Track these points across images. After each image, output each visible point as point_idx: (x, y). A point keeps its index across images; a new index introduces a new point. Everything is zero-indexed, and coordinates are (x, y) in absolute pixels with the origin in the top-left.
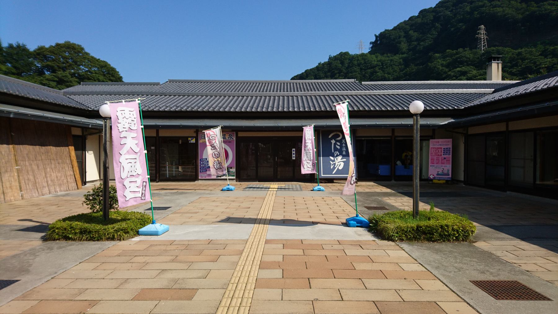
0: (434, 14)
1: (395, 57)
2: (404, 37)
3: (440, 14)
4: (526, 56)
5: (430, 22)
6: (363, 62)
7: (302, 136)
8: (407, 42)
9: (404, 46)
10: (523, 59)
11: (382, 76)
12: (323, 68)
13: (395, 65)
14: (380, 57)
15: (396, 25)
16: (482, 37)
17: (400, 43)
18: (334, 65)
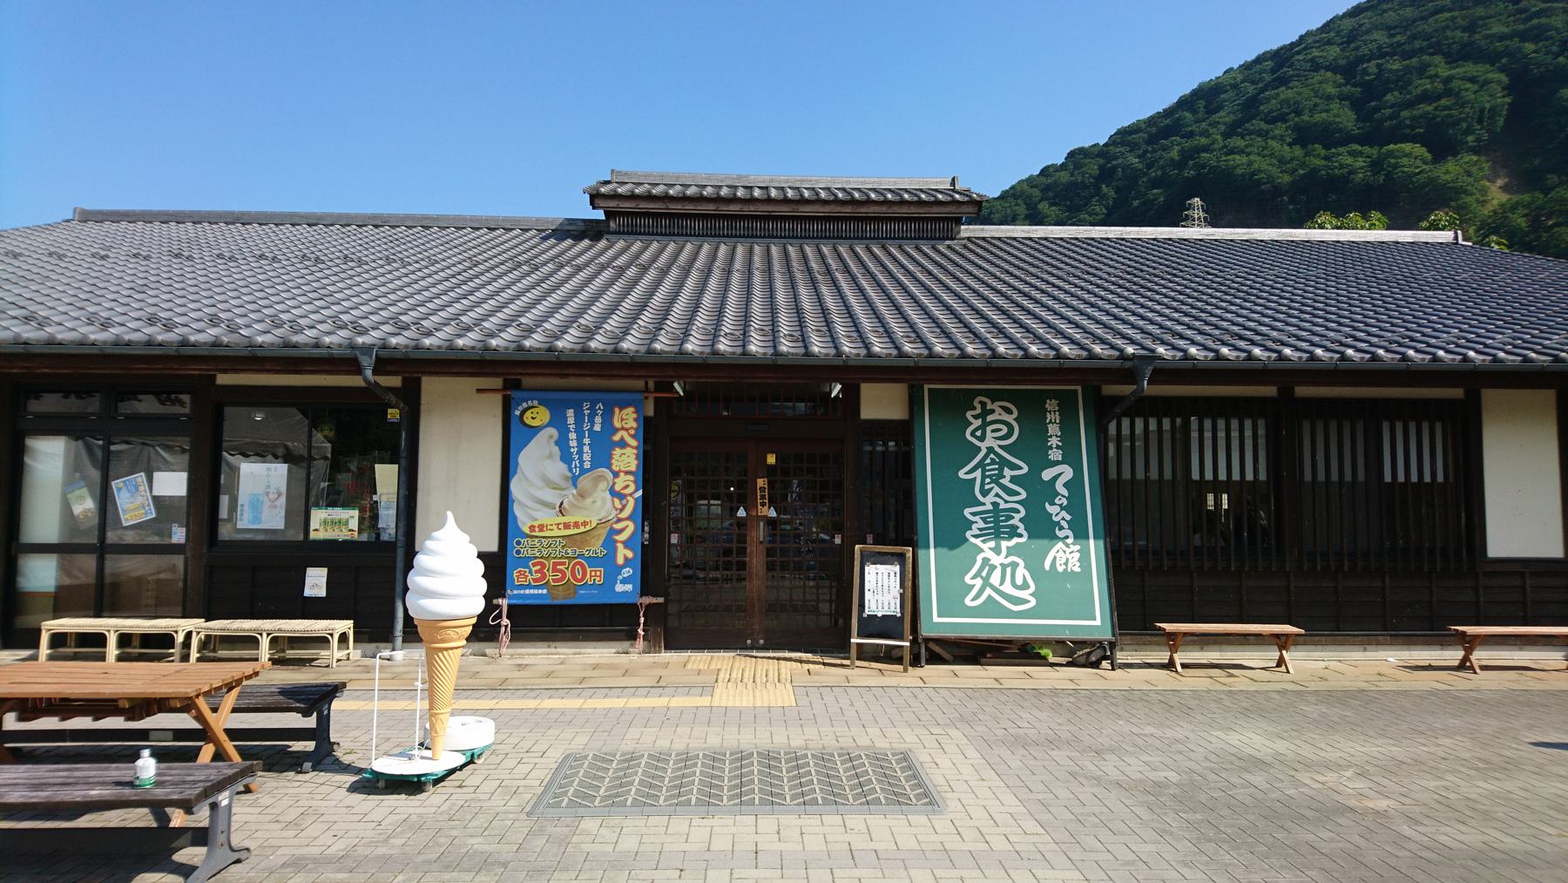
0: (1102, 161)
5: (1092, 180)
7: (289, 637)
15: (1007, 187)
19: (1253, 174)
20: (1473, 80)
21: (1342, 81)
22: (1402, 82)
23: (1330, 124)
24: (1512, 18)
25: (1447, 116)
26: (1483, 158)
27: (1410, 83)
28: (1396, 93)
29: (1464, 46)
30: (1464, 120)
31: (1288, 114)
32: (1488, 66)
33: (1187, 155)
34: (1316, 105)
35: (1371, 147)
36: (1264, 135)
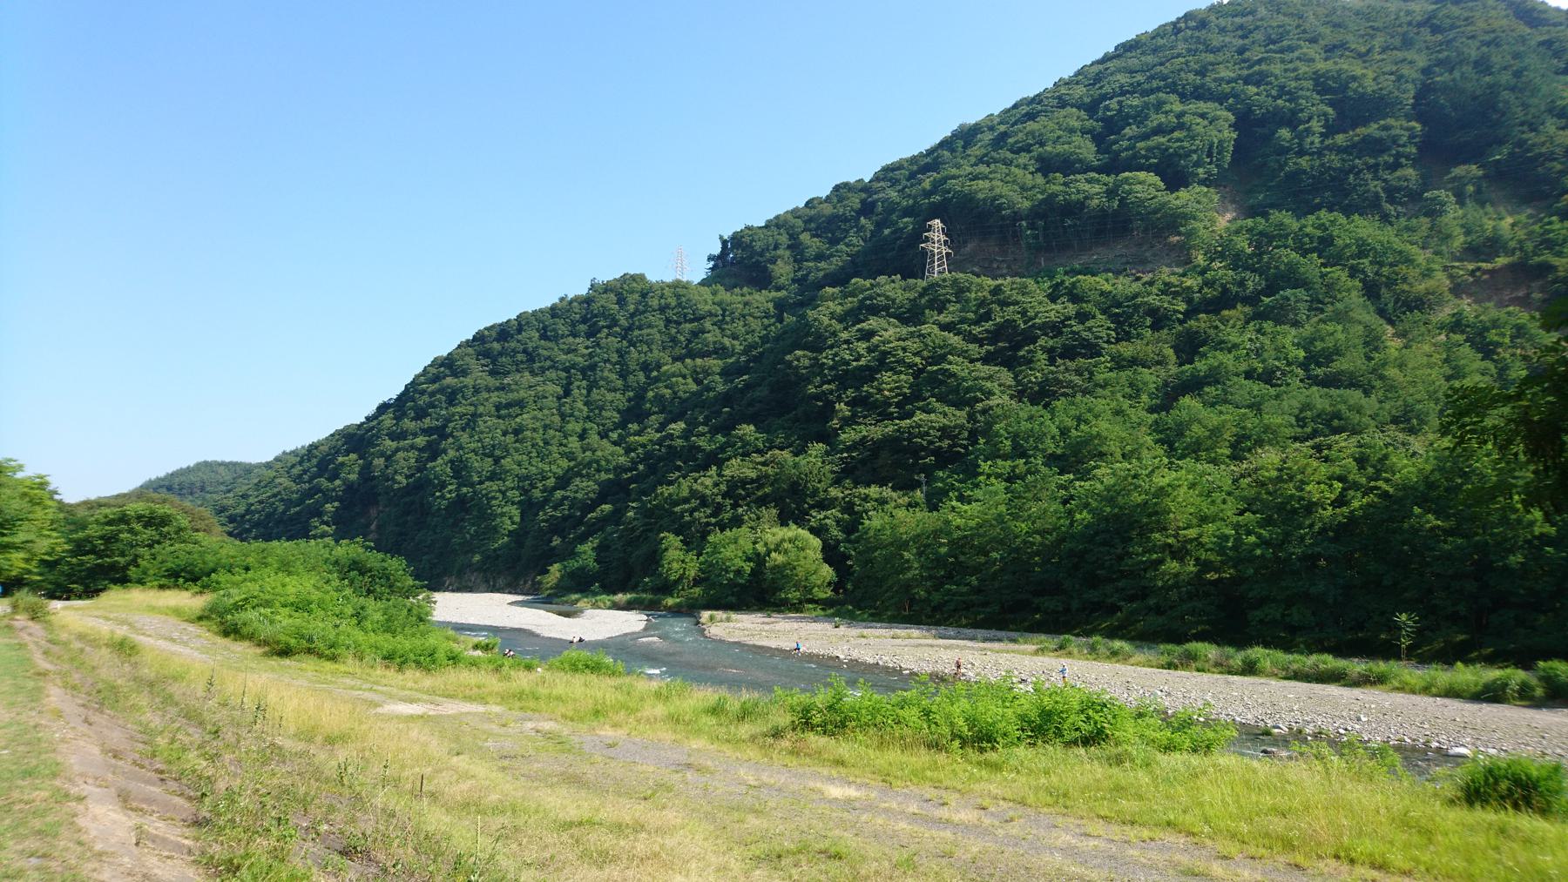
0: (864, 195)
1: (757, 296)
2: (789, 247)
3: (875, 197)
4: (1011, 295)
5: (853, 213)
6: (674, 303)
8: (795, 261)
9: (783, 270)
10: (1004, 304)
11: (715, 343)
12: (569, 311)
13: (754, 317)
14: (724, 295)
16: (936, 251)
17: (774, 263)
18: (599, 305)
19: (995, 199)
20: (1203, 116)
21: (1086, 117)
22: (1140, 117)
23: (1071, 154)
24: (1237, 67)
25: (1179, 147)
26: (1212, 190)
27: (1147, 117)
28: (1134, 127)
29: (1196, 88)
30: (1195, 152)
31: (1031, 145)
32: (1216, 104)
33: (936, 186)
34: (1059, 137)
35: (1108, 175)
36: (1008, 163)
